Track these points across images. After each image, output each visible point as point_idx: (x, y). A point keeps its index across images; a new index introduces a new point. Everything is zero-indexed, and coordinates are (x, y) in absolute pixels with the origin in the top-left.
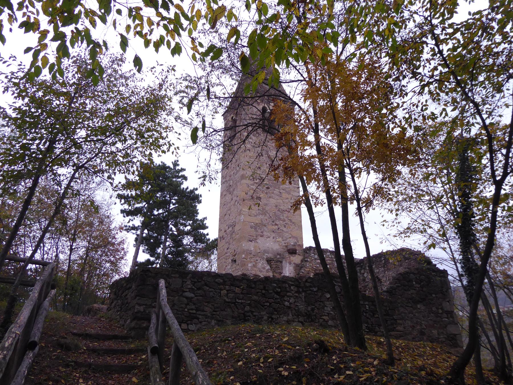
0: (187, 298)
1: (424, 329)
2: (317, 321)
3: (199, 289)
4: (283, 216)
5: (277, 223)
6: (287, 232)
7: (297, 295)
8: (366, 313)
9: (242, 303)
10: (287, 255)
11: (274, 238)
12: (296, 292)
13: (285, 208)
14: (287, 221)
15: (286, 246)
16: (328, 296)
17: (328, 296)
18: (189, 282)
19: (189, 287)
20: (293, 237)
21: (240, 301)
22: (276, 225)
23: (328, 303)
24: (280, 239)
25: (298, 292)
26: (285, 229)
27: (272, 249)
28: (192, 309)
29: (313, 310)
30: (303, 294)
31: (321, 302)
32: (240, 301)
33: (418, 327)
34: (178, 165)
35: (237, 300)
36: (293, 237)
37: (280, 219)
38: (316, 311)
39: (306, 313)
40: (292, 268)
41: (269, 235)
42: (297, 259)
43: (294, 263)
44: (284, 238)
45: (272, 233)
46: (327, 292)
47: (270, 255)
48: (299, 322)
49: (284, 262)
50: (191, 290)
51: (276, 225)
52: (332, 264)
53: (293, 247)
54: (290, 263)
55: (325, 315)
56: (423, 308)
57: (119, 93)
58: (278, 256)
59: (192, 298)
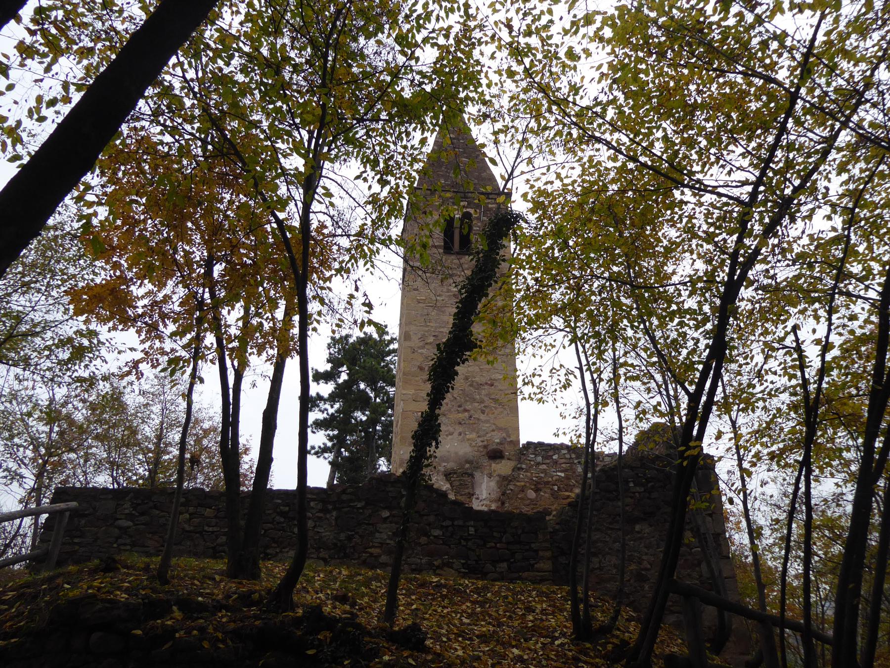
0: (120, 528)
1: (646, 569)
2: (356, 555)
3: (142, 514)
4: (479, 394)
5: (468, 407)
6: (487, 421)
7: (321, 515)
8: (466, 540)
9: (213, 532)
10: (485, 461)
11: (460, 434)
12: (320, 511)
13: (483, 380)
14: (488, 402)
15: (485, 447)
16: (386, 514)
17: (386, 514)
18: (127, 505)
19: (127, 511)
20: (500, 429)
21: (211, 529)
22: (466, 410)
23: (385, 526)
24: (473, 436)
25: (325, 511)
26: (482, 417)
27: (456, 453)
28: (125, 544)
29: (350, 538)
30: (334, 513)
31: (369, 524)
32: (211, 529)
33: (633, 567)
34: (387, 333)
35: (206, 528)
36: (500, 429)
37: (474, 400)
38: (357, 539)
39: (335, 544)
40: (493, 484)
41: (451, 429)
42: (504, 467)
43: (499, 476)
44: (481, 433)
45: (457, 427)
46: (384, 508)
47: (451, 465)
48: (318, 558)
49: (477, 475)
50: (130, 517)
51: (466, 410)
52: (571, 469)
53: (500, 447)
54: (490, 476)
55: (373, 547)
56: (647, 529)
57: (672, 219)
58: (467, 466)
59: (129, 527)
